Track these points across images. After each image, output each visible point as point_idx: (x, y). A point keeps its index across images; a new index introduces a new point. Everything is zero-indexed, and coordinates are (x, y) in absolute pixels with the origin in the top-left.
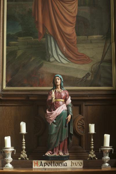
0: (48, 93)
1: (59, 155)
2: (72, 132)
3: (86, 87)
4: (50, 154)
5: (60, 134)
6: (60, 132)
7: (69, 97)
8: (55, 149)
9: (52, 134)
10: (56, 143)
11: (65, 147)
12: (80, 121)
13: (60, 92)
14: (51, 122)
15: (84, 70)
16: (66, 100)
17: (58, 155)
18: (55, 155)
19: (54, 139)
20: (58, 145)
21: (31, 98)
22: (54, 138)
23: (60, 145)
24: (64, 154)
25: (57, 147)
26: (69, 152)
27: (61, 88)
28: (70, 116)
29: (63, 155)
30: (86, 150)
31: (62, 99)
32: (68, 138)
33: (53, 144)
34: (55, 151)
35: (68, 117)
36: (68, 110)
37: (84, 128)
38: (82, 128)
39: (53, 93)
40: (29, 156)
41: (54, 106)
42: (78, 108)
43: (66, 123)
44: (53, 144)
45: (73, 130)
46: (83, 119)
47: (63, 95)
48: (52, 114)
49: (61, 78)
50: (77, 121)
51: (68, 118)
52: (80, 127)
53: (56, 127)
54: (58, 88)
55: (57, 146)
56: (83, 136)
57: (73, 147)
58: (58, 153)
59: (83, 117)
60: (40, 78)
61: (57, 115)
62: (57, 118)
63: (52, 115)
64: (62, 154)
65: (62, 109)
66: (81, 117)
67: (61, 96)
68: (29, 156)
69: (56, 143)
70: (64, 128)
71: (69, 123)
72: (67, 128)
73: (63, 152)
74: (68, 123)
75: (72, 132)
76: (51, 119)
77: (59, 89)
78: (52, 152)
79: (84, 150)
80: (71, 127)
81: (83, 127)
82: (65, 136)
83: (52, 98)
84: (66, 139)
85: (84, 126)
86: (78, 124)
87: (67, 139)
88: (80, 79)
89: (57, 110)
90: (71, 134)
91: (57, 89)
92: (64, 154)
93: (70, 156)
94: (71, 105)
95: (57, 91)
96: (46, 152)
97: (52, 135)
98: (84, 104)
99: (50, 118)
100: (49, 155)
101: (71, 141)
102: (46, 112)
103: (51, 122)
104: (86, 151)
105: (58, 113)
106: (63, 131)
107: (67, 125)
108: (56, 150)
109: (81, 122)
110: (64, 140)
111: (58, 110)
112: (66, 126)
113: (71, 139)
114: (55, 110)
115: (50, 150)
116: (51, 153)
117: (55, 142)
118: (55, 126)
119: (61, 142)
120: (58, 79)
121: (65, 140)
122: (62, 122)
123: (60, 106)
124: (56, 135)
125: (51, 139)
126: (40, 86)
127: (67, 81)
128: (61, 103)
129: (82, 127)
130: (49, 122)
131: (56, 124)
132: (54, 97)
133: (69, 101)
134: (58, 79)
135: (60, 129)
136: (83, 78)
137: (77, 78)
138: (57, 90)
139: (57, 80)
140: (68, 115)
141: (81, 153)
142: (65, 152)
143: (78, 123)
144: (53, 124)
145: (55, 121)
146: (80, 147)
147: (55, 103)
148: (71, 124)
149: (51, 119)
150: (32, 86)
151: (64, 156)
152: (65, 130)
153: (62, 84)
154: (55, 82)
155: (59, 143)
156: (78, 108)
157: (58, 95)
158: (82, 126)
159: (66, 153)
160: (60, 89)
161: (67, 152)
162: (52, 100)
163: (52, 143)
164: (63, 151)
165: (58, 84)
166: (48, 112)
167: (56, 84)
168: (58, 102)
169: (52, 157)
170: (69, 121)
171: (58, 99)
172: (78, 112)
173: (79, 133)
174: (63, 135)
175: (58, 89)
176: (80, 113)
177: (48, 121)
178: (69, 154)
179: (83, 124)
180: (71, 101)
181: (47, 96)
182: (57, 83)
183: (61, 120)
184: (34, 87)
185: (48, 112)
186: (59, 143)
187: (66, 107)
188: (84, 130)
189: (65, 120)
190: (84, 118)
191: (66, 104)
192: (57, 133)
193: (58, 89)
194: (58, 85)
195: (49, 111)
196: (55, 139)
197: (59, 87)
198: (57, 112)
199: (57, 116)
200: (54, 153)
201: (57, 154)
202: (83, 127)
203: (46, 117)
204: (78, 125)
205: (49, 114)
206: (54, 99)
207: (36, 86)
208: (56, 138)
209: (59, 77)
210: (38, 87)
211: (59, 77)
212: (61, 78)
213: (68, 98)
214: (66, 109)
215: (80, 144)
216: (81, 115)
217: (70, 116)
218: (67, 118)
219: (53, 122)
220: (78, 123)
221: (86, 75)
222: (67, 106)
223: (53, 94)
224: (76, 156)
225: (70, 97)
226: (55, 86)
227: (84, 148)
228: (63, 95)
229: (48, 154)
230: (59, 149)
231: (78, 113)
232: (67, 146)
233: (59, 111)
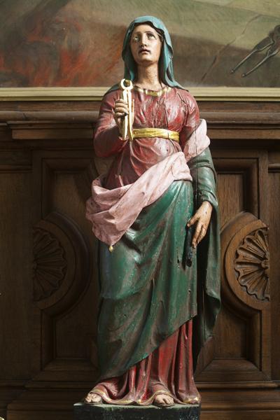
0: (98, 112)
1: (155, 402)
2: (215, 292)
3: (271, 87)
4: (108, 399)
5: (159, 298)
6: (157, 288)
7: (198, 124)
8: (133, 374)
9: (118, 296)
10: (135, 346)
11: (182, 365)
12: (249, 240)
13: (159, 94)
14: (114, 240)
15: (260, 15)
16: (184, 135)
17: (146, 404)
18: (134, 403)
19: (127, 326)
20: (147, 353)
21: (18, 135)
22: (130, 320)
23: (156, 352)
24: (178, 397)
25: (143, 363)
26: (199, 389)
27: (161, 79)
28: (205, 212)
29: (175, 402)
30: (274, 378)
31: (166, 126)
32: (196, 321)
33: (125, 348)
34: (152, 281)
35: (197, 216)
36: (196, 184)
37: (265, 275)
38: (257, 275)
39: (125, 93)
40: (10, 406)
41: (124, 160)
42: (236, 180)
43: (188, 243)
44: (125, 348)
45: (218, 280)
46: (261, 233)
47: (174, 110)
48: (118, 197)
49: (161, 32)
50: (237, 239)
51: (197, 222)
52: (250, 269)
53: (139, 265)
54: (146, 76)
55: (145, 357)
56: (260, 311)
57: (213, 366)
58: (150, 393)
59: (260, 224)
60: (65, 45)
61: (146, 205)
62: (145, 218)
63: (122, 203)
64: (170, 400)
65: (165, 175)
66: (251, 223)
67: (162, 113)
68: (10, 406)
69: (135, 346)
70: (177, 268)
71: (203, 245)
72: (192, 271)
73: (170, 388)
74: (198, 246)
75: (215, 292)
76: (113, 221)
77: (152, 84)
78: (119, 389)
79: (265, 380)
80: (211, 263)
81: (261, 269)
82: (182, 310)
83: (123, 118)
84: (187, 323)
85: (267, 264)
86: (237, 255)
87: (191, 322)
88: (243, 52)
89: (144, 178)
90: (209, 299)
91: (141, 83)
92: (178, 397)
93: (202, 406)
94: (210, 159)
95: (141, 91)
96: (88, 390)
97: (119, 303)
98: (265, 164)
99: (112, 217)
100: (104, 402)
101: (207, 334)
102: (89, 193)
103: (114, 240)
104: (274, 385)
105: (149, 193)
106: (175, 285)
107: (194, 257)
108: (140, 382)
109: (251, 245)
110: (175, 328)
111: (151, 177)
112: (186, 262)
113: (211, 324)
114: (132, 178)
115: (108, 380)
116: (115, 392)
117: (133, 337)
118: (135, 257)
119: (161, 338)
120: (149, 35)
121: (180, 329)
122: (171, 238)
123: (156, 159)
124: (140, 307)
125: (117, 321)
126: (61, 81)
127: (190, 61)
128: (162, 146)
129: (256, 268)
130: (104, 239)
131: (138, 251)
132: (132, 115)
133: (201, 139)
134: (149, 35)
135: (157, 275)
136: (259, 46)
137: (229, 48)
138: (144, 87)
139: (145, 37)
140: (197, 204)
141: (251, 394)
142: (182, 387)
143: (240, 252)
144: (123, 247)
145: (132, 235)
146: (251, 366)
147: (137, 146)
148: (211, 248)
149: (113, 221)
150: (25, 83)
151: (178, 406)
152: (184, 278)
153: (168, 59)
154: (135, 48)
155: (155, 345)
156: (236, 180)
157: (149, 108)
158: (259, 265)
159: (189, 392)
160: (156, 82)
161: (193, 387)
162: (118, 130)
163: (119, 343)
164: (173, 383)
165: (148, 57)
166: (98, 190)
167: (136, 56)
168: (151, 140)
169: (117, 410)
170: (204, 234)
171: (151, 126)
172: (235, 200)
173: (244, 300)
174: (174, 303)
175: (150, 82)
176: (249, 203)
177: (97, 234)
178: (202, 398)
179: (261, 254)
180: (207, 142)
181: (94, 124)
182: (142, 50)
183: (163, 228)
184: (37, 85)
185: (98, 190)
186: (151, 343)
187: (187, 168)
188: (269, 286)
189: (183, 230)
190: (266, 229)
191: (187, 155)
192: (144, 296)
193: (150, 82)
194: (149, 63)
195: (104, 186)
196: (134, 322)
197: (153, 71)
198: (144, 189)
199: (144, 209)
200: (127, 392)
201: (144, 399)
202: (261, 269)
203: (89, 217)
204: (240, 259)
205: (104, 198)
206: (129, 122)
207: (46, 85)
208: (140, 320)
209: (150, 24)
210: (54, 85)
211: (150, 24)
212: (161, 32)
213: (196, 127)
214: (188, 176)
215: (248, 353)
216: (250, 217)
217: (205, 212)
218: (192, 221)
219: (125, 239)
220: (240, 252)
221: (272, 35)
222: (193, 163)
223: (125, 100)
224: (228, 406)
225: (204, 123)
226: (135, 69)
227: (266, 367)
228: (174, 110)
229: (97, 399)
230: (154, 375)
231: (237, 206)
232: (191, 361)
233: (153, 184)
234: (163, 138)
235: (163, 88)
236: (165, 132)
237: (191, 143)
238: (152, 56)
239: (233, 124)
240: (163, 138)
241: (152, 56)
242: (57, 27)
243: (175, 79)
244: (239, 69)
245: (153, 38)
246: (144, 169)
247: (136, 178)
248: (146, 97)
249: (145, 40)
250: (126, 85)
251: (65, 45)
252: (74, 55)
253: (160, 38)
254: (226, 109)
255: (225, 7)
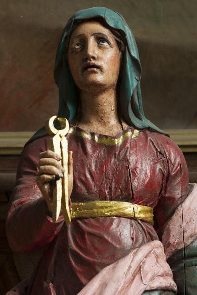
49: (119, 35)
134: (100, 39)
139: (92, 42)
160: (113, 121)
165: (99, 78)
175: (103, 122)
193: (103, 122)
194: (101, 88)
197: (108, 101)
209: (101, 20)
212: (119, 35)
235: (125, 132)
245: (106, 44)
249: (92, 48)
253: (118, 44)
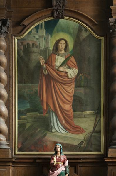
16: (64, 163)
27: (61, 154)
31: (61, 162)
36: (66, 171)
47: (62, 159)
48: (53, 173)
49: (60, 147)
60: (45, 145)
63: (54, 174)
77: (59, 155)
88: (75, 146)
102: (49, 172)
105: (58, 173)
114: (56, 170)
120: (59, 147)
123: (59, 167)
126: (44, 151)
128: (61, 165)
133: (67, 163)
134: (59, 147)
136: (78, 145)
137: (73, 145)
139: (58, 147)
150: (38, 151)
154: (56, 149)
160: (60, 154)
162: (53, 163)
165: (58, 151)
166: (51, 172)
168: (59, 164)
181: (50, 159)
182: (57, 150)
185: (51, 172)
194: (59, 152)
195: (51, 171)
197: (59, 153)
205: (51, 173)
207: (41, 151)
212: (60, 147)
214: (65, 170)
221: (81, 142)
222: (65, 167)
226: (56, 152)
228: (62, 159)
234: (61, 164)
236: (61, 163)
237: (65, 164)
238: (59, 151)
239: (32, 22)
240: (61, 164)
241: (59, 151)
242: (43, 141)
243: (45, 28)
244: (82, 167)
246: (58, 169)
247: (56, 170)
248: (58, 157)
250: (55, 157)
251: (45, 145)
252: (46, 146)
254: (57, 111)
255: (72, 138)
